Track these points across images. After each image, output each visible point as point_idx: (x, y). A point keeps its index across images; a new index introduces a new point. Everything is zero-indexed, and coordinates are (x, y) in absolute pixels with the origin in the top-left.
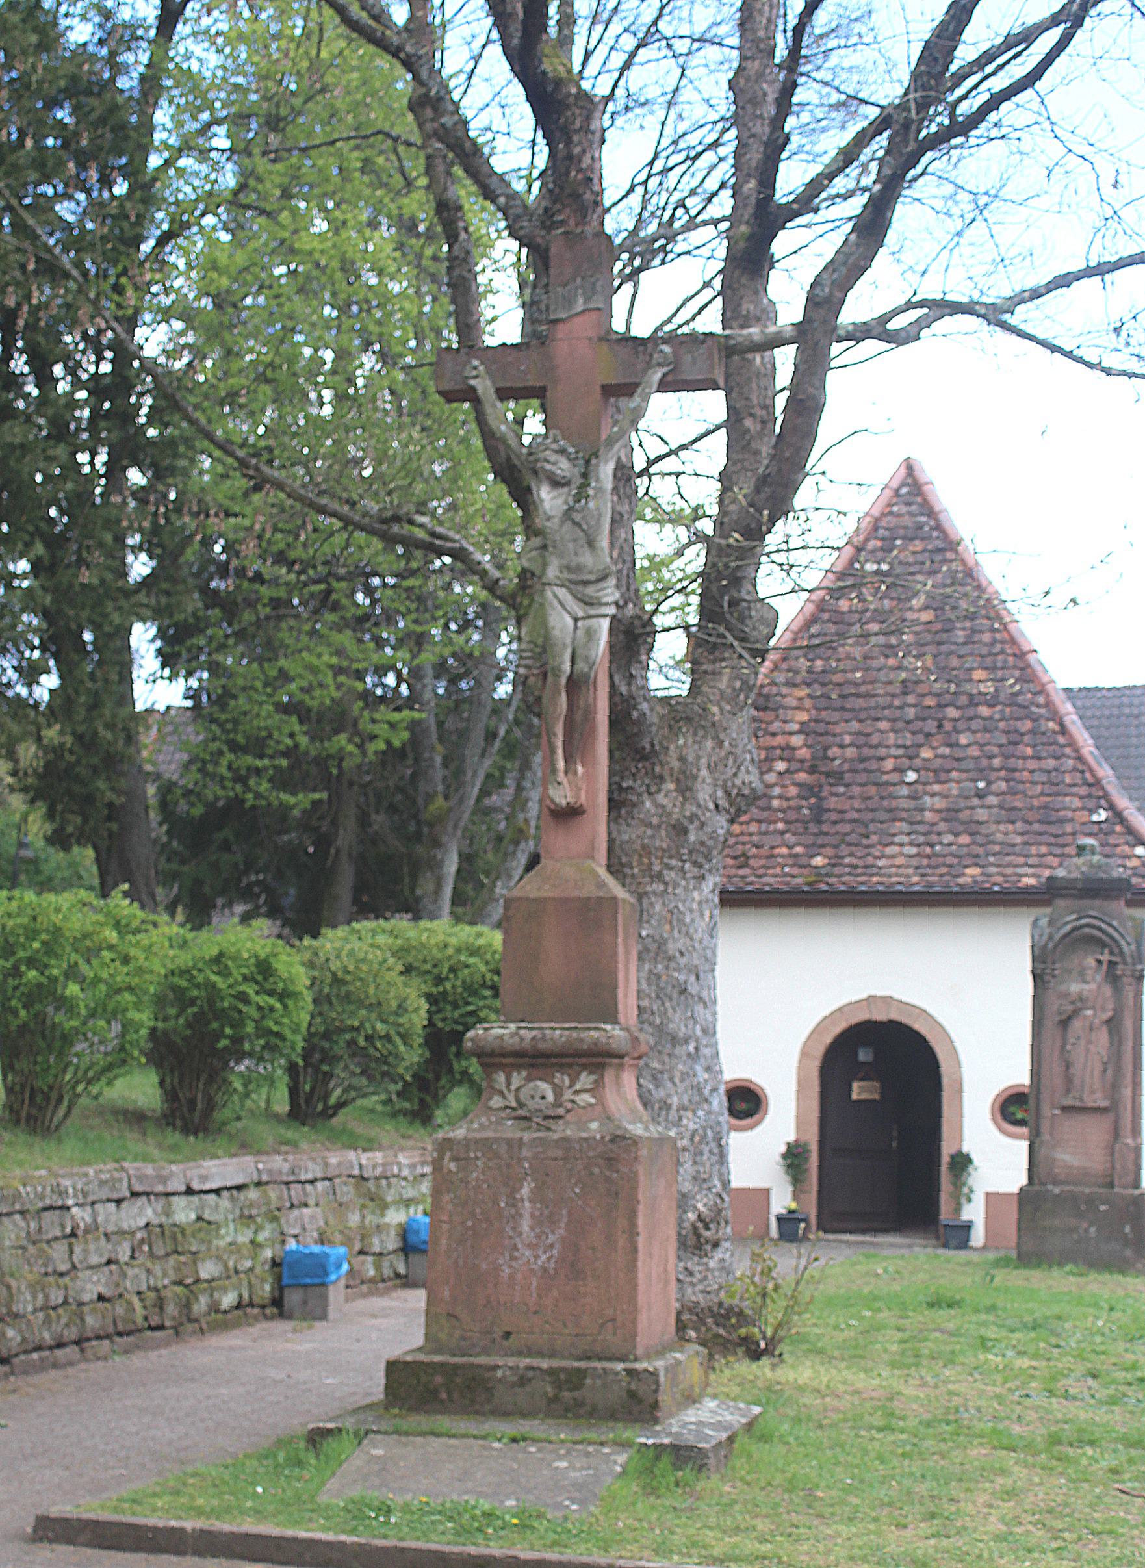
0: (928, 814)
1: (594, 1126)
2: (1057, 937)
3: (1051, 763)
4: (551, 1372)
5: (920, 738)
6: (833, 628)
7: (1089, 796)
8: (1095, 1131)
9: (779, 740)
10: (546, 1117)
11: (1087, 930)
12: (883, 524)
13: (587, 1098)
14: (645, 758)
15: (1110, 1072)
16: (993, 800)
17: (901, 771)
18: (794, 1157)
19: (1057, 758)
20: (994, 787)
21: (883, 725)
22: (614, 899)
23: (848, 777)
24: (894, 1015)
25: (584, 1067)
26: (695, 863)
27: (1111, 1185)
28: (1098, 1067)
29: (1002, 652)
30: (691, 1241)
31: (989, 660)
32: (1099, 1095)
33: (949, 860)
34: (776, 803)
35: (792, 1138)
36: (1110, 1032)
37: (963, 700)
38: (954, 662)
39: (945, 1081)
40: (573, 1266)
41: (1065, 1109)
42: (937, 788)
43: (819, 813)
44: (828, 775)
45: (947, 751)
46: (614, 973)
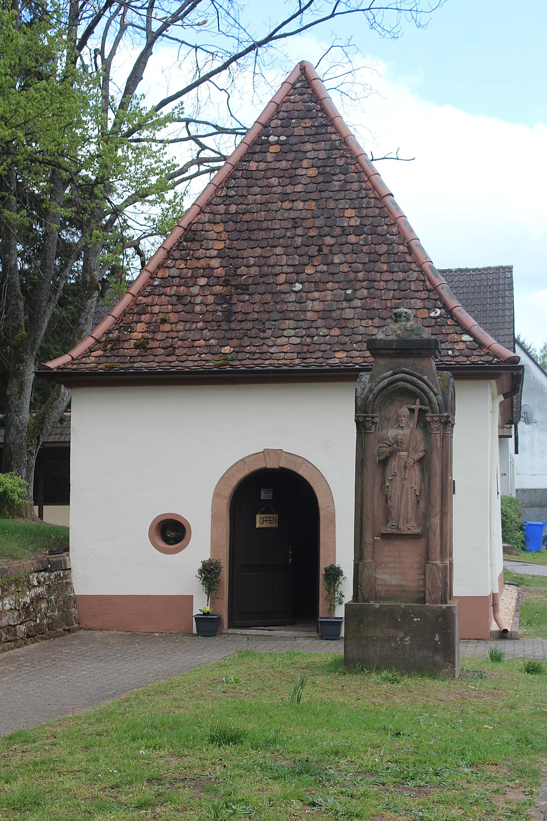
0: (309, 314)
5: (305, 259)
6: (244, 182)
8: (409, 555)
9: (203, 263)
11: (401, 383)
12: (283, 108)
15: (422, 504)
16: (357, 303)
18: (209, 572)
20: (358, 294)
21: (279, 250)
24: (283, 464)
27: (423, 600)
28: (411, 499)
31: (356, 203)
32: (413, 524)
33: (323, 347)
34: (198, 308)
35: (207, 557)
36: (422, 470)
37: (338, 231)
38: (332, 204)
39: (322, 513)
41: (384, 536)
42: (316, 295)
43: (229, 316)
44: (237, 287)
45: (325, 268)
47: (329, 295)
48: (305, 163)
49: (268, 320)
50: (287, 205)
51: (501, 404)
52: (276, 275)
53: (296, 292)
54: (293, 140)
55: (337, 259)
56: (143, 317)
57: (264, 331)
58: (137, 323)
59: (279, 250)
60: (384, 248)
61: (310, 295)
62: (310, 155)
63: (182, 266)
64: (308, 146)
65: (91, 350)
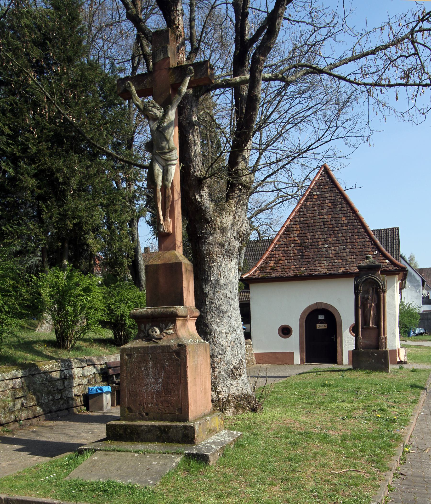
1: (172, 341)
3: (363, 240)
5: (329, 236)
9: (292, 239)
14: (209, 222)
23: (310, 247)
26: (228, 256)
33: (336, 266)
40: (167, 389)
42: (333, 248)
45: (335, 238)
48: (327, 201)
50: (322, 217)
54: (322, 193)
55: (340, 235)
60: (357, 230)
62: (329, 198)
64: (328, 195)
65: (256, 271)
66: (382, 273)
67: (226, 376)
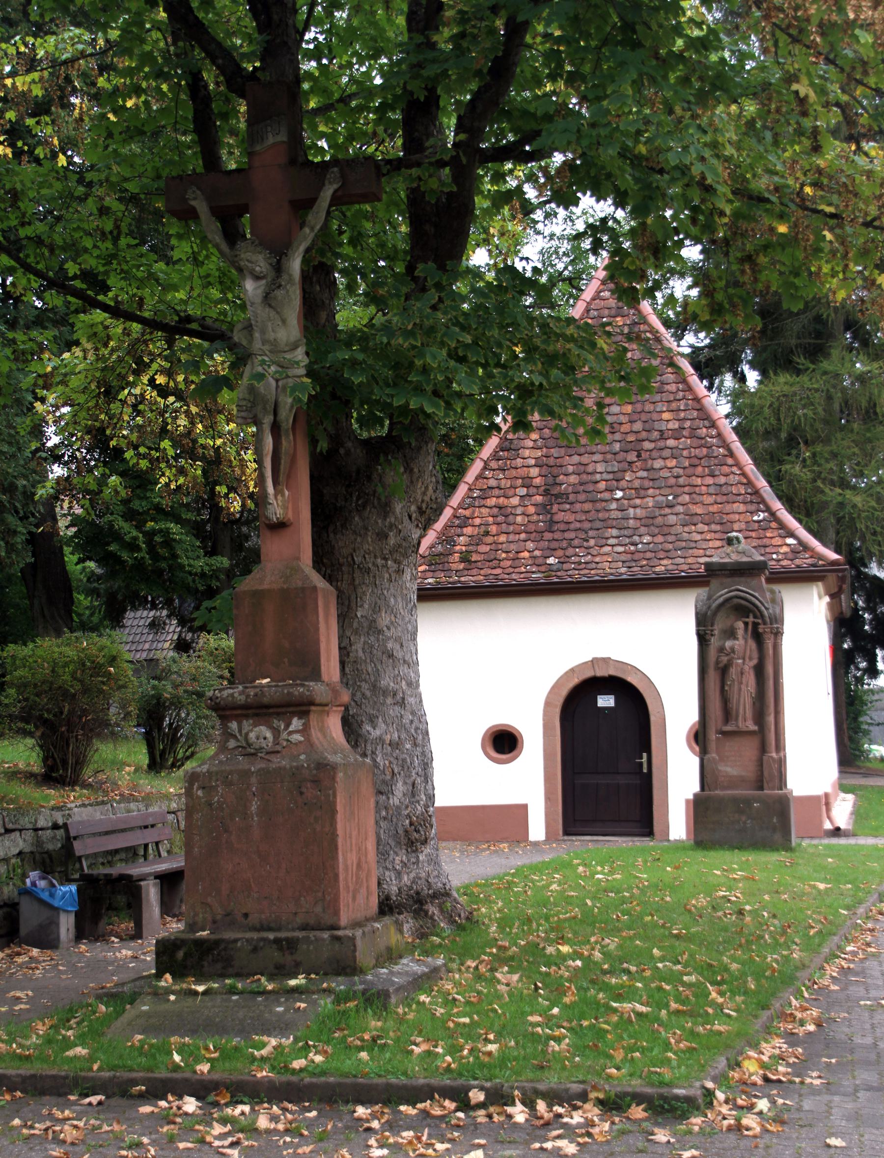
2: (714, 605)
3: (722, 480)
4: (277, 941)
5: (626, 465)
7: (751, 502)
10: (267, 753)
13: (298, 737)
17: (611, 490)
19: (726, 475)
20: (680, 499)
22: (315, 588)
23: (572, 497)
24: (612, 672)
25: (294, 714)
26: (395, 561)
29: (684, 398)
30: (404, 840)
37: (656, 435)
39: (653, 718)
41: (724, 733)
42: (638, 501)
44: (557, 496)
45: (644, 474)
46: (317, 642)
47: (650, 502)
49: (591, 529)
51: (828, 604)
52: (597, 482)
53: (617, 500)
56: (465, 530)
57: (587, 541)
58: (459, 536)
59: (597, 457)
61: (632, 502)
63: (501, 476)
66: (769, 581)
67: (393, 844)
